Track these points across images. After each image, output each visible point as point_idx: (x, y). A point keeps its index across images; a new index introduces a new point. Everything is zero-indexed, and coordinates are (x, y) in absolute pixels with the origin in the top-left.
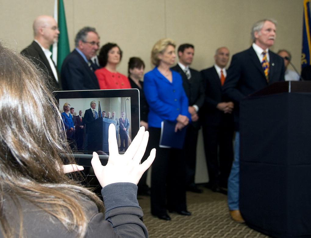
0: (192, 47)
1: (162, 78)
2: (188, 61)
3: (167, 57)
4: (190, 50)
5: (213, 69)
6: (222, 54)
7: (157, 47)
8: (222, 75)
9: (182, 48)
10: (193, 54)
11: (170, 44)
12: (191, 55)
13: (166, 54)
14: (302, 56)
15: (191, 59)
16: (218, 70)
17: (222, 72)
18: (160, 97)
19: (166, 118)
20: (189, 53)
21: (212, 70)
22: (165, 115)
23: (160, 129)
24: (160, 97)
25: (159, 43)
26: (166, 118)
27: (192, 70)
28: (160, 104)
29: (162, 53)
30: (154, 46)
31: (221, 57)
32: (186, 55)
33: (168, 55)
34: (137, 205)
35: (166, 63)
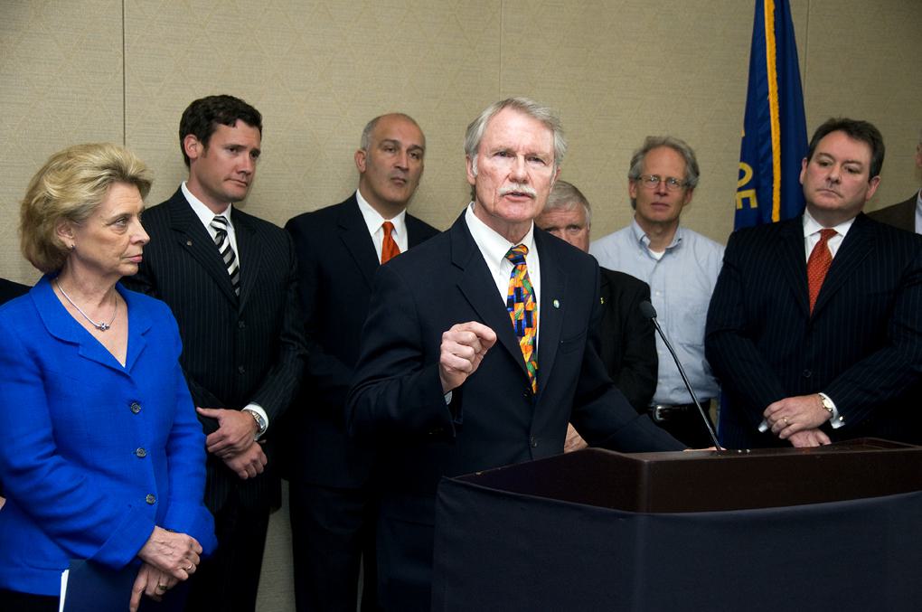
0: (253, 118)
1: (78, 342)
2: (231, 189)
3: (102, 240)
4: (238, 132)
5: (347, 214)
6: (394, 147)
7: (51, 188)
8: (390, 244)
9: (205, 118)
10: (255, 153)
11: (118, 173)
12: (243, 159)
13: (98, 227)
14: (742, 174)
15: (247, 179)
16: (373, 220)
17: (388, 228)
18: (63, 443)
19: (89, 551)
20: (235, 149)
21: (347, 214)
22: (81, 536)
23: (58, 598)
24: (63, 443)
25: (60, 163)
26: (89, 551)
27: (243, 222)
28: (62, 476)
29: (74, 218)
30: (36, 187)
31: (387, 159)
32: (224, 162)
33: (109, 233)
34: (63, 460)
35: (92, 265)
